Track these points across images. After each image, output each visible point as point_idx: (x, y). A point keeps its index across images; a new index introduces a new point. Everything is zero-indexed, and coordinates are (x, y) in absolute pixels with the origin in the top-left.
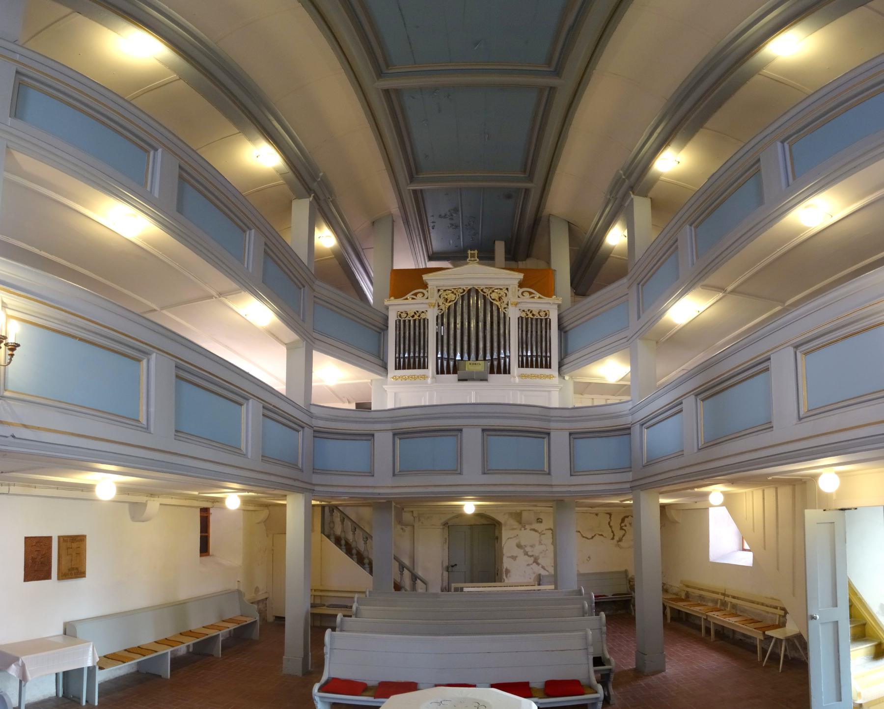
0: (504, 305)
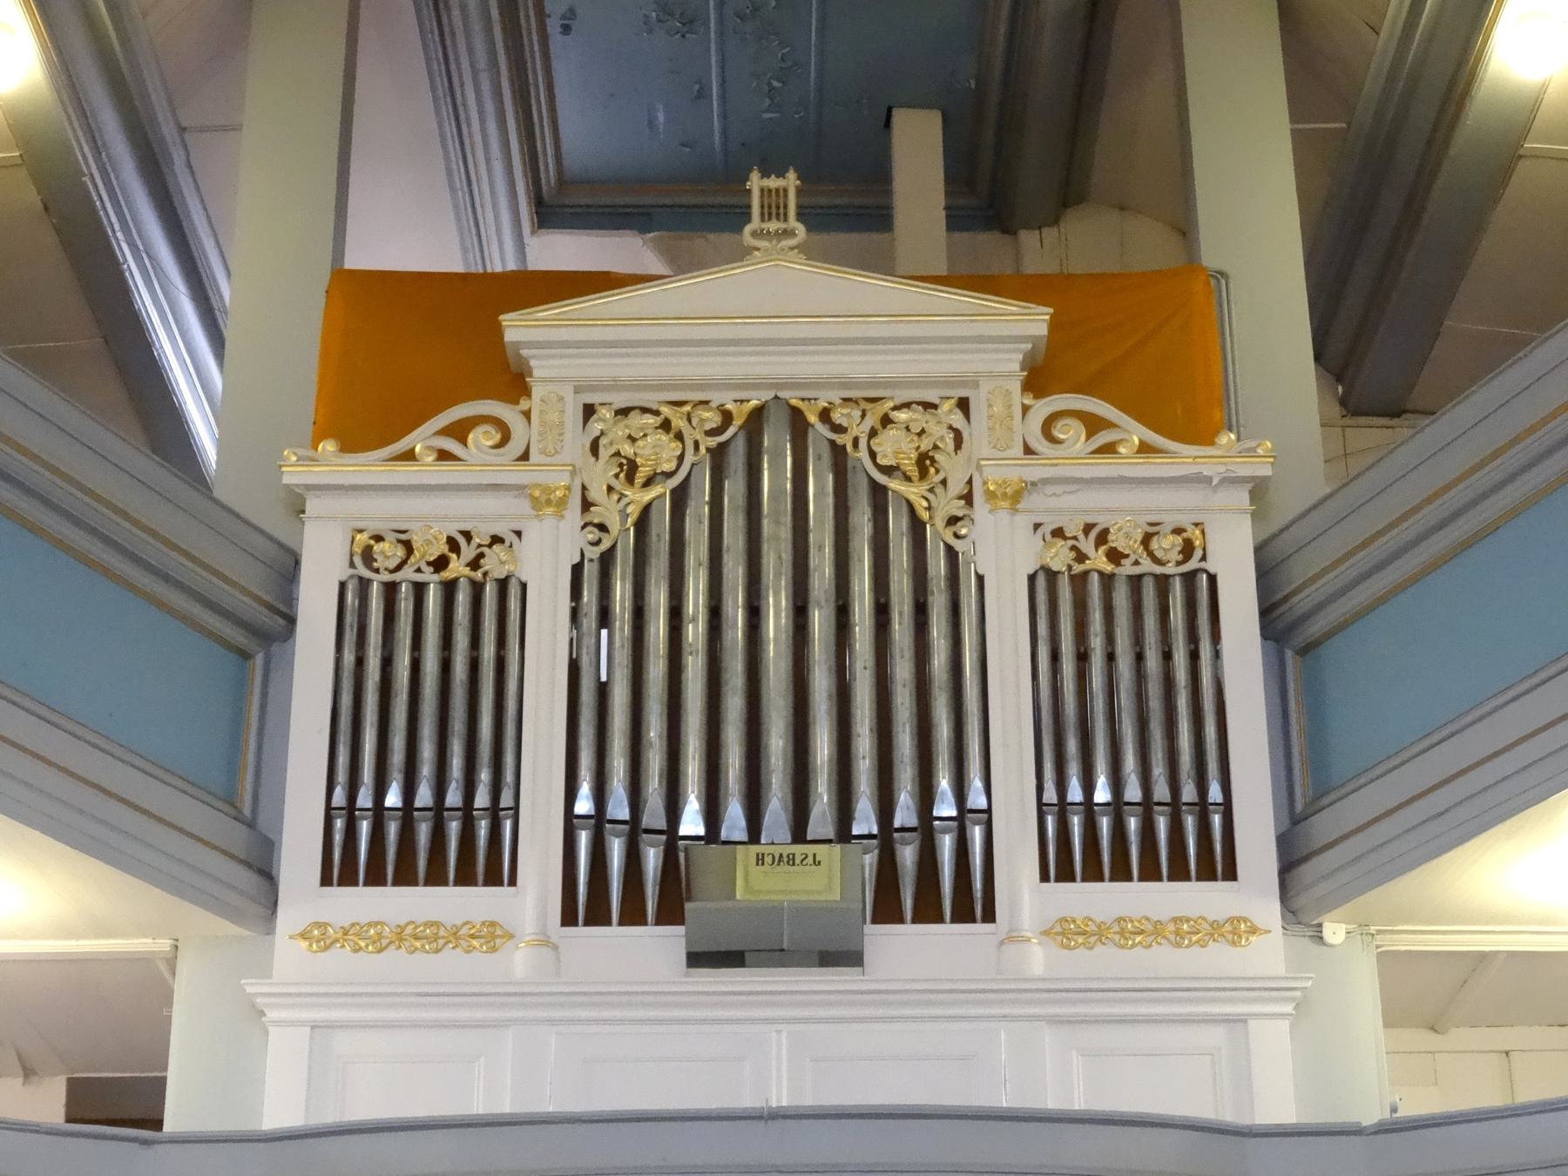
0: (949, 504)
